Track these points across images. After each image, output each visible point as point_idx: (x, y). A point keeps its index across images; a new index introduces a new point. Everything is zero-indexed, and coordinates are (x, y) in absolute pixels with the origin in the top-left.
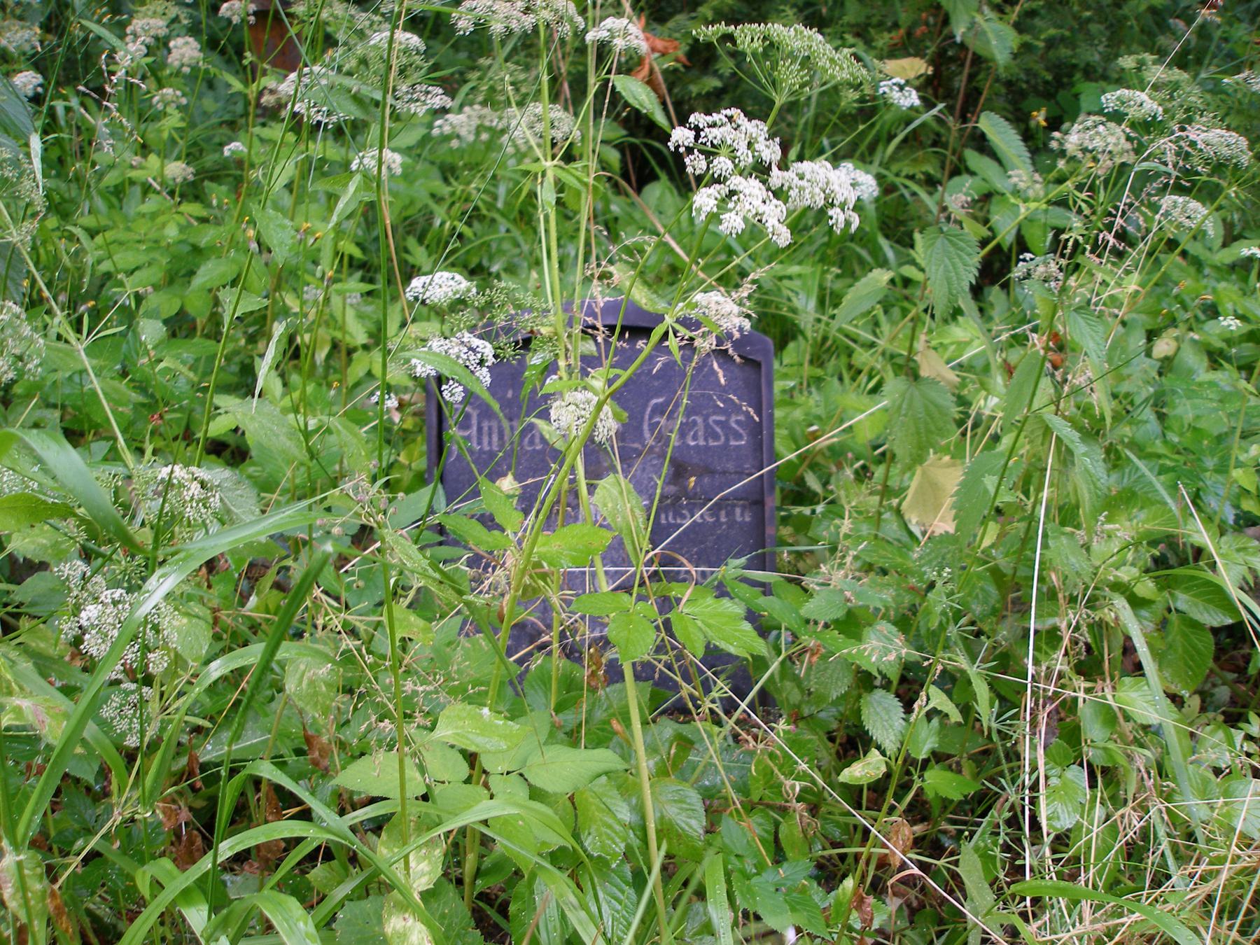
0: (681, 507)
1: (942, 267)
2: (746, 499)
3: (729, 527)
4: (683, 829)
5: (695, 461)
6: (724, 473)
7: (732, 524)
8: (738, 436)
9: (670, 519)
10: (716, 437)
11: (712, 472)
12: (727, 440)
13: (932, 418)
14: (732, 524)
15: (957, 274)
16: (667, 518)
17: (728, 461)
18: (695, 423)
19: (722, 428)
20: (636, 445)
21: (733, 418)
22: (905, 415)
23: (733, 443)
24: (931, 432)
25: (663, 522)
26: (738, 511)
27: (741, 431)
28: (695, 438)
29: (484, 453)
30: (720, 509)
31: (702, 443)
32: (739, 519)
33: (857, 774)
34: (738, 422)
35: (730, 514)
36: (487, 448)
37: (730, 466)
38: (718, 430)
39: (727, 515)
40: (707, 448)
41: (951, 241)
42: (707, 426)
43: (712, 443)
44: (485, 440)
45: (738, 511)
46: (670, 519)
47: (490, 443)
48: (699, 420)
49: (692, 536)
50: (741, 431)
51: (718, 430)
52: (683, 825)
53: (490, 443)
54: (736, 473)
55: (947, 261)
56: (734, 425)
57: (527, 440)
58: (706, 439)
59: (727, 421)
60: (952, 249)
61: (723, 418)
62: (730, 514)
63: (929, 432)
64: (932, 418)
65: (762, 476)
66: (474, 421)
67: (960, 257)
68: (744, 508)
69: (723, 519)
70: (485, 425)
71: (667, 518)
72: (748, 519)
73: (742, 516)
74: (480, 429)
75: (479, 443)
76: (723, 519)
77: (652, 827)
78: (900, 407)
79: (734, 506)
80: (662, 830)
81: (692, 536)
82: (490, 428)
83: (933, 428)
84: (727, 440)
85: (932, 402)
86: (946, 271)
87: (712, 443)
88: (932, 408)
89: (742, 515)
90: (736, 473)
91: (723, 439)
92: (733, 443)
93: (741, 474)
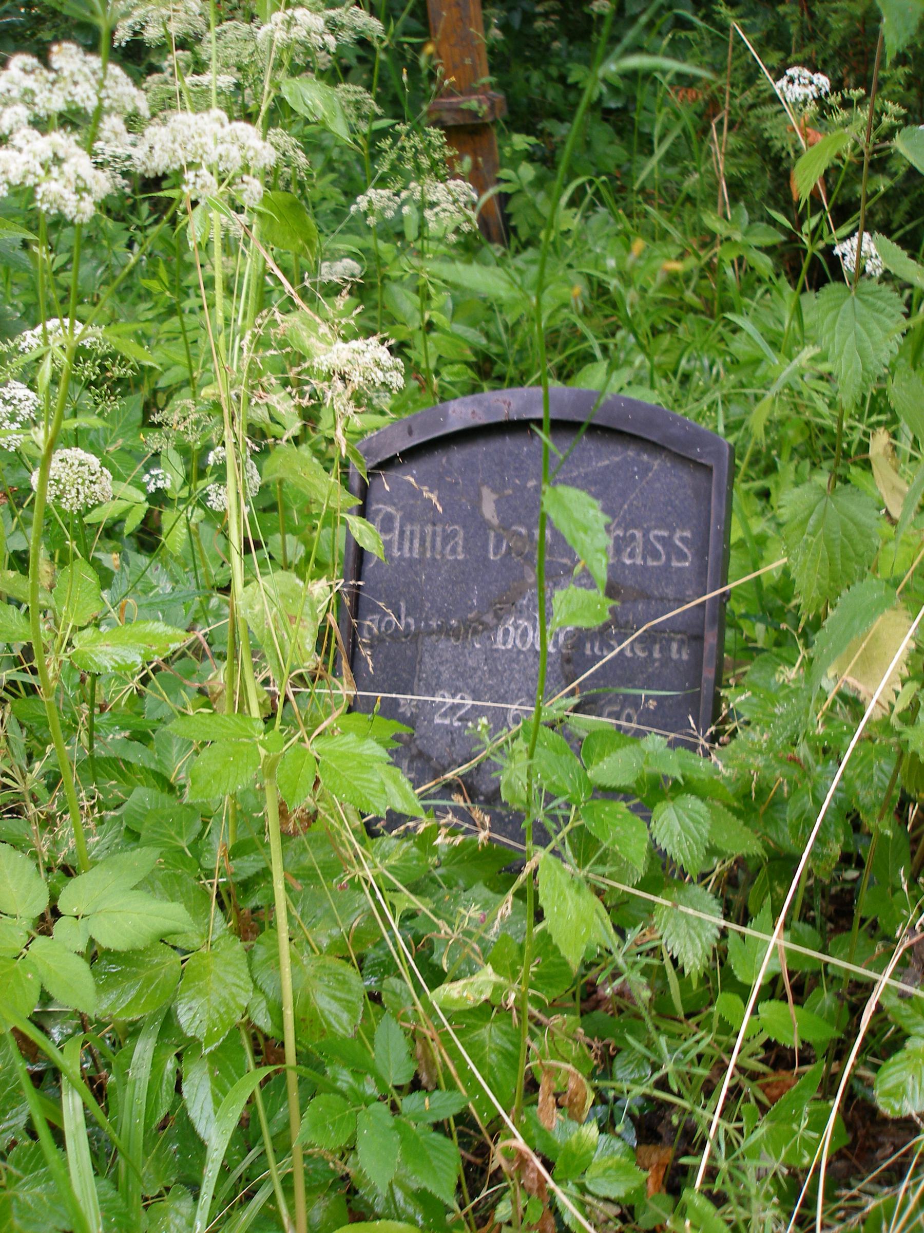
0: (610, 636)
1: (852, 336)
2: (683, 632)
3: (662, 665)
4: (329, 1024)
5: (630, 582)
6: (662, 599)
7: (666, 660)
8: (682, 556)
9: (596, 650)
10: (656, 555)
11: (648, 598)
12: (669, 559)
13: (850, 541)
14: (666, 660)
15: (873, 343)
16: (592, 649)
17: (667, 585)
18: (633, 537)
19: (664, 546)
20: (565, 561)
21: (678, 534)
22: (813, 534)
23: (675, 564)
24: (849, 559)
25: (588, 652)
26: (675, 646)
27: (686, 550)
28: (632, 555)
29: (404, 560)
30: (654, 642)
31: (639, 561)
32: (674, 656)
33: (455, 995)
34: (682, 539)
35: (665, 649)
36: (407, 555)
37: (670, 592)
38: (659, 547)
39: (661, 650)
40: (645, 568)
41: (864, 301)
42: (647, 541)
43: (651, 563)
44: (407, 545)
45: (675, 646)
46: (596, 650)
47: (411, 549)
48: (638, 534)
49: (619, 672)
50: (686, 550)
51: (659, 547)
52: (331, 1019)
53: (411, 549)
54: (675, 600)
55: (858, 326)
56: (678, 543)
57: (449, 548)
58: (644, 558)
59: (671, 537)
60: (865, 311)
61: (665, 534)
62: (665, 649)
63: (846, 558)
64: (850, 541)
65: (702, 605)
66: (397, 524)
67: (878, 322)
68: (682, 643)
69: (657, 655)
70: (408, 529)
71: (592, 649)
72: (685, 657)
73: (679, 653)
74: (402, 533)
75: (400, 549)
76: (657, 655)
77: (289, 1013)
78: (805, 521)
79: (670, 640)
80: (303, 1020)
81: (619, 672)
82: (412, 533)
83: (852, 554)
84: (669, 559)
85: (852, 519)
86: (858, 339)
87: (651, 563)
88: (850, 526)
89: (679, 651)
90: (675, 600)
91: (664, 558)
92: (675, 564)
93: (681, 601)
